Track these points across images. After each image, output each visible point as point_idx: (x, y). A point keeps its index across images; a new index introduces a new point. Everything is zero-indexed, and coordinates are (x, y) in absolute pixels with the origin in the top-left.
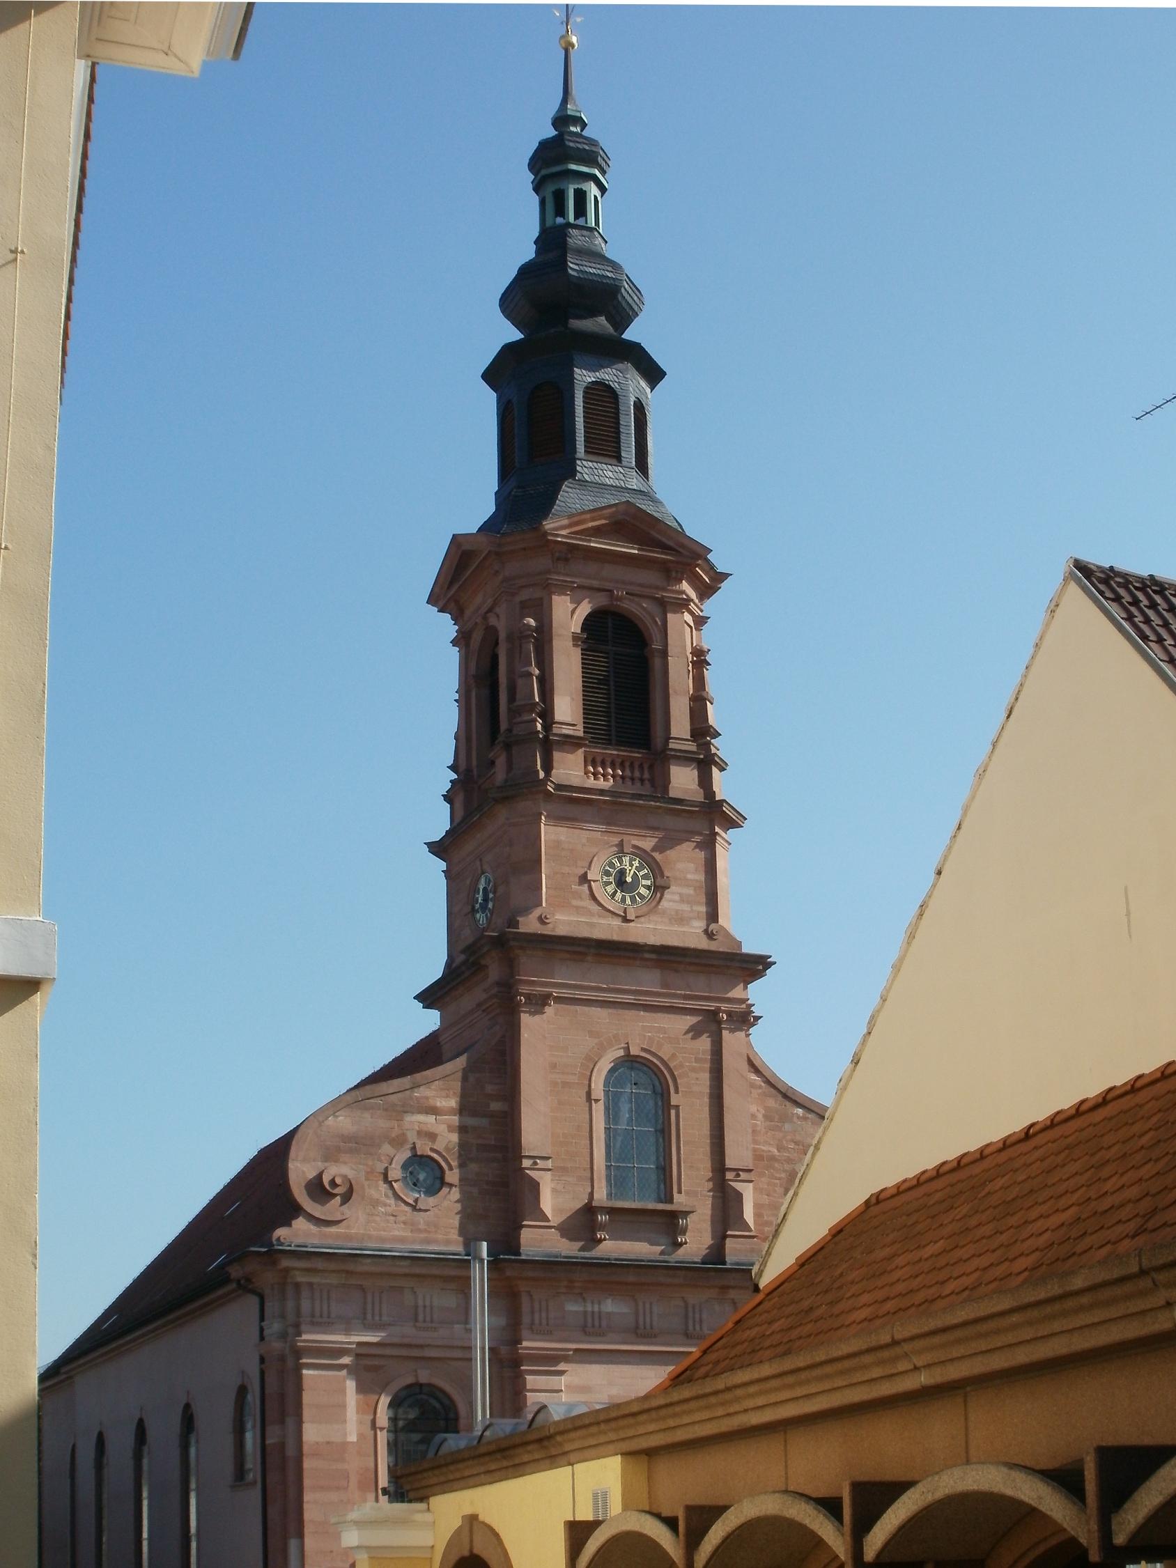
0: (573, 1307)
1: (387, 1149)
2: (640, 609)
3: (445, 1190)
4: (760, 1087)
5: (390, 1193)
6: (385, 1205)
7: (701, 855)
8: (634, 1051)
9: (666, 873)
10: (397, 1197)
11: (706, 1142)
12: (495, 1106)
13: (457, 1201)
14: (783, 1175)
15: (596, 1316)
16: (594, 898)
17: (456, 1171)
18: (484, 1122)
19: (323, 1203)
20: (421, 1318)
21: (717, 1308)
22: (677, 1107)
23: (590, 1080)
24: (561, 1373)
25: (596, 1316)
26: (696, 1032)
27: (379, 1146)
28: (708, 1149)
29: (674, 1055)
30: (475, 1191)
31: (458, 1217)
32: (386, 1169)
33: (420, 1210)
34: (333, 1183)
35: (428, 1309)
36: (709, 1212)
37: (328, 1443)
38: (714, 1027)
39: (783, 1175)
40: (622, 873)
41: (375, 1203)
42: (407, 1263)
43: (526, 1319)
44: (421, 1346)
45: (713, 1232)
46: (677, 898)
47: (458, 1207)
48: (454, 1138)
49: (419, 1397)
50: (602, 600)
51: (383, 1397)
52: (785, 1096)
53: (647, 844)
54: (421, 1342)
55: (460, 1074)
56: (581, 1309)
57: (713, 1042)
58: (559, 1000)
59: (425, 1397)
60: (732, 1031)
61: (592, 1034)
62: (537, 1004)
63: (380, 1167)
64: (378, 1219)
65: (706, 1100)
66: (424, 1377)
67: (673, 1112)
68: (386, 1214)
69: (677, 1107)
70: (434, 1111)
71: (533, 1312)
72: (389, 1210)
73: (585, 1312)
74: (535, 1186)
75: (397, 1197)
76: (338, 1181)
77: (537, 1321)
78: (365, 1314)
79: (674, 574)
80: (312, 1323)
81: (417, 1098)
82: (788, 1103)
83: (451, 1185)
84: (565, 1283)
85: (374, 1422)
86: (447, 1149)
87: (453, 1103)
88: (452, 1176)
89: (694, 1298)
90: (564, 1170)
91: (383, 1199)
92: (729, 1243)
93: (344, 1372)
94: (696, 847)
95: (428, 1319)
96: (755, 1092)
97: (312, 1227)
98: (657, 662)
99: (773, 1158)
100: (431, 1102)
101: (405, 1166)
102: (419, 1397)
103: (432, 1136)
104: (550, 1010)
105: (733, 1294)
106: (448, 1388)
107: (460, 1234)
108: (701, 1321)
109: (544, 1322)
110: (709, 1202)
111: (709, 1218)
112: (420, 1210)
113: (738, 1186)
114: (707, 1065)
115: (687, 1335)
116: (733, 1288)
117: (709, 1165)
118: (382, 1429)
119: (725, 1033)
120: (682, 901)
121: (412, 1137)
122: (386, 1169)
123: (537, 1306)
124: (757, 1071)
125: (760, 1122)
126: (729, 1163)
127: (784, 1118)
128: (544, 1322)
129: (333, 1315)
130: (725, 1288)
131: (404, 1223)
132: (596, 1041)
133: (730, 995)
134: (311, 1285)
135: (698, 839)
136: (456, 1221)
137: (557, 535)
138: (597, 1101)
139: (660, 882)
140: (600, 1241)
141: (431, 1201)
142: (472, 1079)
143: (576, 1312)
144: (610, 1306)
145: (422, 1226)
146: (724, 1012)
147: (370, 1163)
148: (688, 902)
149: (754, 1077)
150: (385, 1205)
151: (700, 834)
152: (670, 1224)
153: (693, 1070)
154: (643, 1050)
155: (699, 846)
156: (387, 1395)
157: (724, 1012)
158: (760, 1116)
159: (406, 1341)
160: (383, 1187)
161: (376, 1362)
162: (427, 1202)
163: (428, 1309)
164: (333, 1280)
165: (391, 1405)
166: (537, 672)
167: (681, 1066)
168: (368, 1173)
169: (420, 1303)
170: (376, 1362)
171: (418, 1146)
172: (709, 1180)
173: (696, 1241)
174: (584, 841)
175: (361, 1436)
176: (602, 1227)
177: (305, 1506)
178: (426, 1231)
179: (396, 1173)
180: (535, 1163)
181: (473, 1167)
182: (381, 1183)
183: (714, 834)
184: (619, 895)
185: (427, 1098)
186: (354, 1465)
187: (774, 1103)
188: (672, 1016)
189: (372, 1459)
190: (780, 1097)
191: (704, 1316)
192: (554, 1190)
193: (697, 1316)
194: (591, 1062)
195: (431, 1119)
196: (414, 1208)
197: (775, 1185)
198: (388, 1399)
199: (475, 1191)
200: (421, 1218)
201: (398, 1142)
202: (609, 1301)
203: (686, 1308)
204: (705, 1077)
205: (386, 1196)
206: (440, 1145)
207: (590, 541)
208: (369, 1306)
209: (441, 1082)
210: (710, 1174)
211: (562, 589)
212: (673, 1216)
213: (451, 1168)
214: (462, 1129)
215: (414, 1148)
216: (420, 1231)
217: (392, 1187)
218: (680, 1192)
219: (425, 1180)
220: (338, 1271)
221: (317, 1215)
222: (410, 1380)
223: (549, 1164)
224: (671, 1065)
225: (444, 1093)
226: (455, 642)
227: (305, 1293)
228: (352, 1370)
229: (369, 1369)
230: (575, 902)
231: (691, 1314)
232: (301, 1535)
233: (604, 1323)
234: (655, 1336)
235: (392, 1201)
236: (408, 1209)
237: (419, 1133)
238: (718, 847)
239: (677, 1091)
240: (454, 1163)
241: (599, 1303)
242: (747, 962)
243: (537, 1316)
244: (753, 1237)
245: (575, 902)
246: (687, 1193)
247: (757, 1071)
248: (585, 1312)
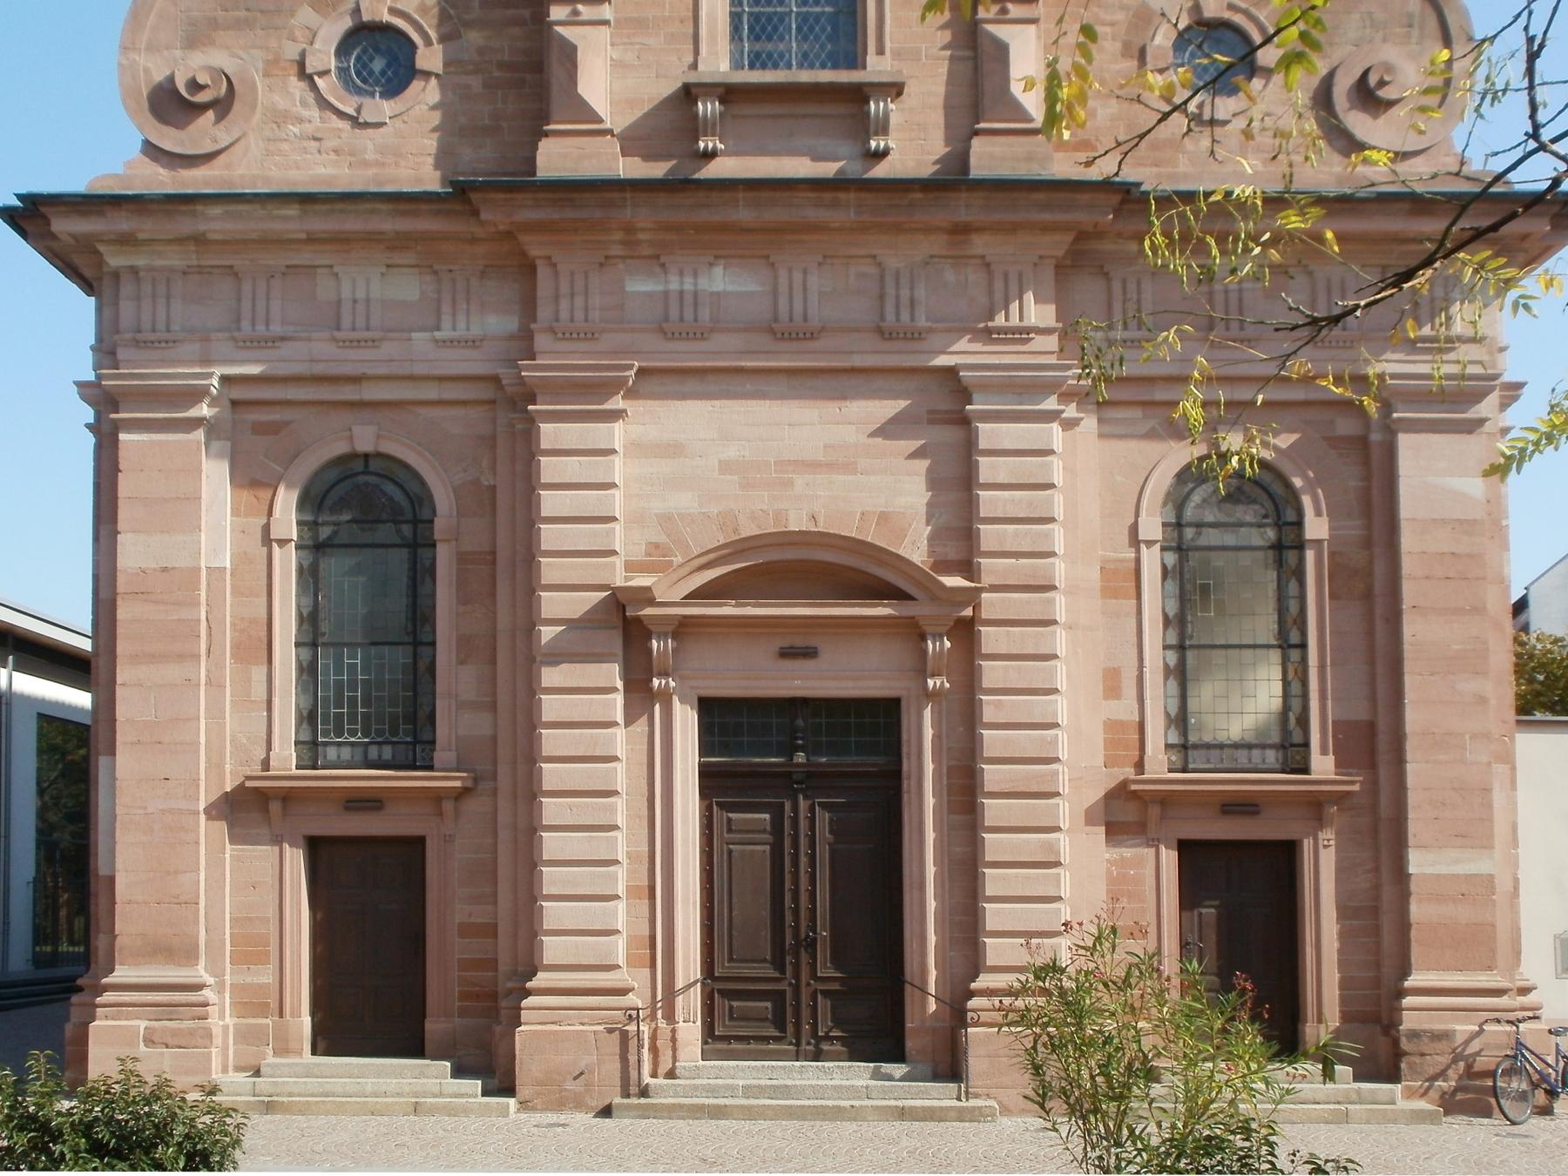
0: (640, 285)
3: (417, 85)
5: (310, 98)
6: (301, 120)
10: (324, 104)
13: (434, 108)
15: (689, 300)
17: (438, 48)
19: (181, 125)
20: (346, 321)
21: (950, 276)
24: (616, 415)
25: (689, 300)
30: (475, 83)
31: (436, 135)
32: (303, 54)
33: (367, 125)
34: (195, 86)
35: (361, 308)
36: (941, 90)
37: (165, 570)
39: (1120, 16)
41: (280, 118)
42: (292, 211)
43: (544, 312)
44: (356, 380)
45: (948, 126)
47: (436, 118)
49: (362, 479)
51: (281, 490)
54: (348, 369)
56: (660, 288)
59: (372, 479)
63: (291, 51)
64: (285, 146)
66: (365, 439)
68: (302, 137)
71: (557, 298)
73: (666, 293)
75: (324, 104)
76: (203, 79)
77: (564, 315)
78: (238, 320)
80: (137, 343)
83: (427, 75)
84: (618, 236)
85: (266, 529)
88: (430, 57)
89: (898, 256)
90: (640, 24)
93: (200, 435)
95: (361, 322)
97: (161, 170)
101: (343, 49)
102: (362, 479)
105: (980, 244)
106: (412, 459)
107: (437, 166)
108: (912, 303)
109: (579, 315)
110: (943, 69)
111: (940, 101)
112: (367, 125)
113: (1001, 31)
115: (883, 333)
118: (283, 542)
122: (303, 54)
123: (564, 288)
128: (579, 315)
129: (175, 327)
130: (961, 231)
131: (335, 151)
134: (134, 270)
136: (431, 143)
140: (710, 155)
141: (387, 107)
143: (649, 295)
144: (719, 280)
145: (370, 156)
147: (273, 44)
150: (301, 120)
152: (852, 107)
156: (289, 486)
159: (319, 369)
160: (297, 87)
161: (274, 416)
162: (380, 108)
163: (361, 308)
164: (173, 259)
165: (302, 504)
168: (267, 63)
169: (346, 293)
170: (274, 416)
173: (911, 142)
175: (240, 559)
176: (707, 128)
177: (119, 691)
178: (378, 164)
179: (324, 56)
181: (474, 37)
182: (294, 80)
186: (220, 614)
189: (264, 599)
191: (921, 293)
192: (617, 65)
193: (905, 293)
196: (355, 121)
198: (294, 496)
199: (475, 83)
200: (368, 141)
202: (718, 271)
203: (882, 278)
205: (304, 103)
208: (246, 305)
212: (858, 95)
213: (428, 43)
216: (366, 164)
217: (314, 87)
218: (881, 51)
219: (383, 73)
220: (180, 241)
221: (167, 146)
222: (341, 448)
227: (127, 289)
228: (212, 428)
229: (260, 429)
231: (890, 290)
232: (112, 751)
233: (705, 314)
234: (812, 336)
235: (314, 113)
236: (345, 125)
240: (433, 34)
241: (695, 275)
243: (564, 304)
244: (1035, 132)
246: (897, 54)
248: (666, 293)
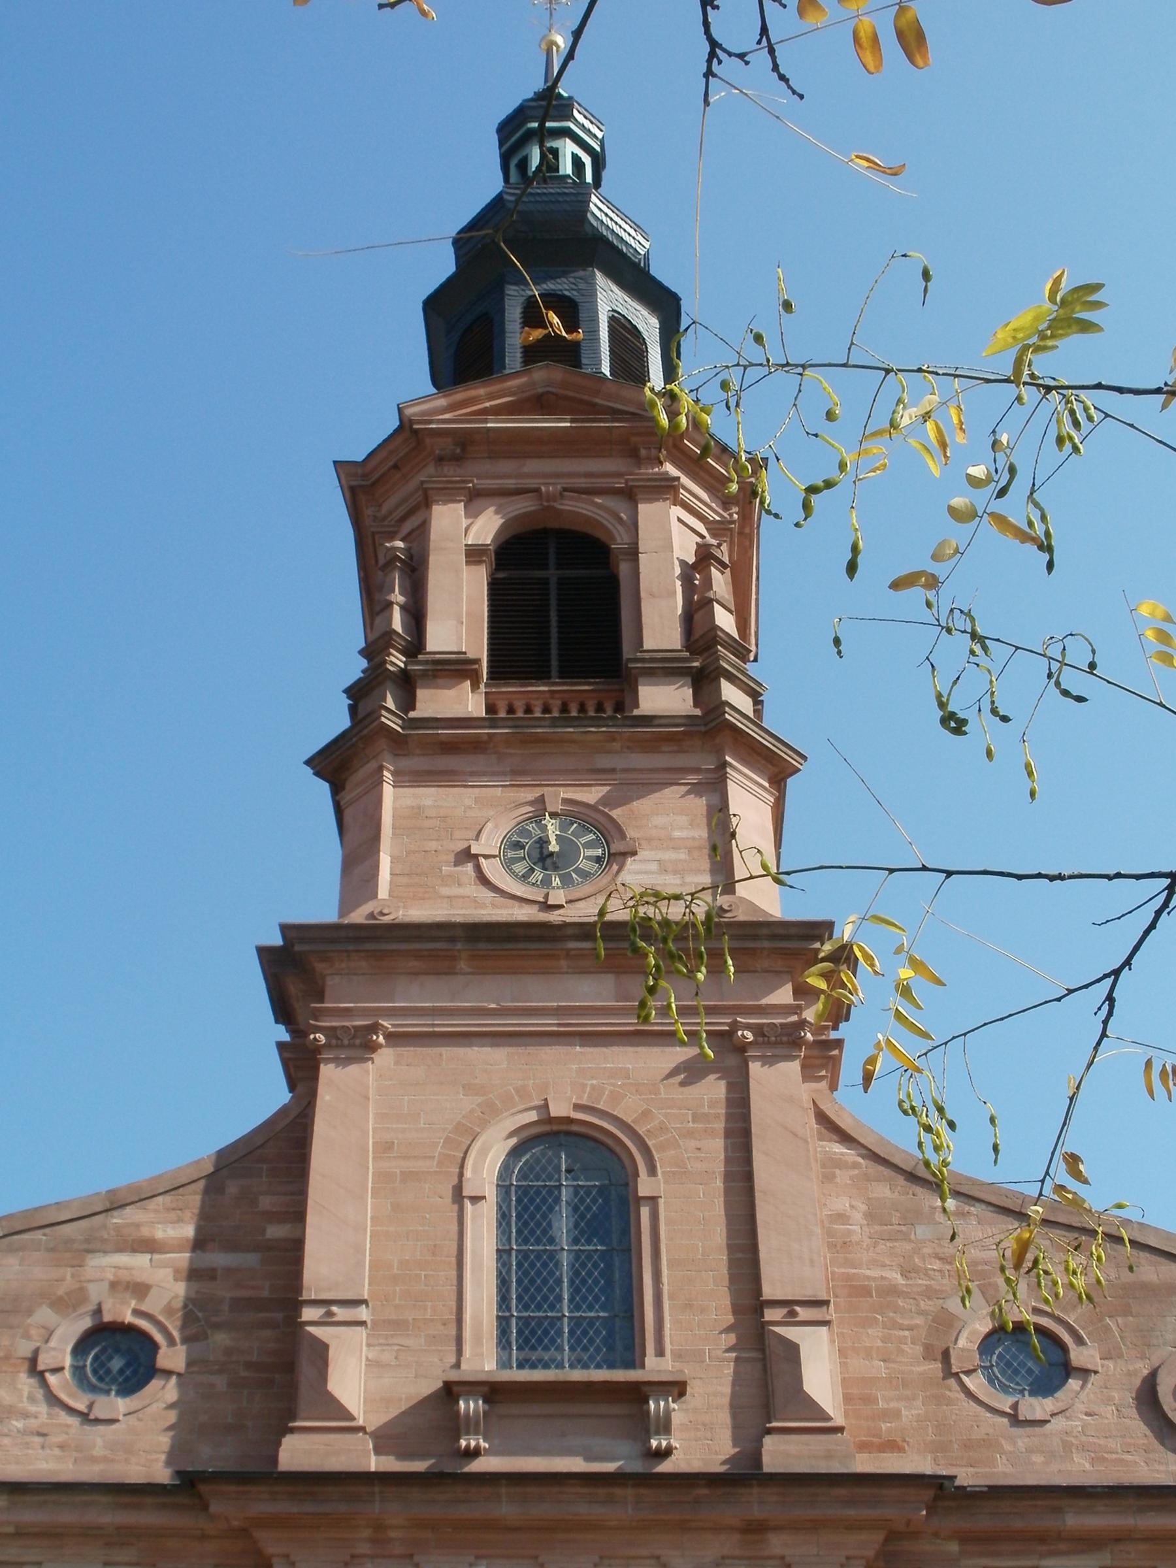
1: (44, 1315)
2: (593, 510)
4: (856, 1165)
5: (39, 1394)
6: (26, 1415)
7: (699, 804)
8: (556, 1110)
9: (631, 833)
11: (721, 1261)
12: (275, 1231)
14: (919, 1321)
16: (484, 880)
18: (250, 1260)
22: (653, 1200)
23: (462, 1166)
26: (691, 1072)
27: (30, 1312)
28: (725, 1271)
29: (646, 1114)
32: (36, 1352)
33: (97, 1421)
36: (727, 1390)
38: (732, 1061)
39: (919, 1321)
40: (543, 842)
46: (654, 867)
48: (180, 1289)
50: (523, 505)
52: (912, 1177)
53: (591, 795)
55: (201, 1184)
57: (730, 1087)
58: (394, 1038)
60: (768, 1061)
61: (469, 1089)
62: (351, 1046)
63: (24, 1348)
65: (719, 1183)
67: (645, 1212)
68: (25, 1432)
69: (653, 1200)
70: (149, 1246)
72: (33, 1423)
74: (321, 1351)
79: (643, 452)
81: (118, 1228)
82: (919, 1190)
83: (168, 1373)
84: (366, 1533)
86: (169, 1311)
87: (188, 1231)
88: (172, 1357)
90: (398, 1325)
91: (26, 1405)
92: (769, 1442)
94: (688, 792)
96: (843, 1177)
98: (624, 568)
99: (893, 1290)
100: (145, 1232)
101: (81, 1347)
103: (141, 1290)
104: (385, 1057)
111: (726, 1401)
112: (97, 1421)
113: (790, 1333)
114: (720, 1125)
116: (777, 1529)
117: (726, 1302)
119: (755, 1067)
120: (664, 870)
121: (97, 1292)
122: (36, 1352)
124: (845, 1138)
125: (857, 1228)
126: (769, 1291)
127: (912, 1217)
130: (755, 1529)
131: (61, 1447)
132: (480, 1099)
133: (765, 1001)
135: (693, 779)
136: (165, 1440)
137: (430, 422)
138: (475, 1199)
139: (617, 847)
141: (122, 1405)
142: (232, 1188)
145: (98, 1451)
146: (748, 1027)
148: (675, 872)
149: (838, 1149)
150: (26, 1415)
151: (696, 770)
153: (690, 1134)
154: (577, 1107)
155: (696, 789)
157: (748, 1027)
158: (858, 1216)
160: (26, 1383)
166: (401, 599)
167: (662, 1129)
171: (106, 1308)
172: (728, 1330)
173: (697, 1437)
174: (469, 802)
178: (105, 1459)
180: (330, 1314)
183: (724, 765)
184: (538, 875)
185: (138, 1226)
187: (887, 1190)
188: (642, 1050)
190: (901, 1180)
194: (465, 1137)
195: (142, 1260)
197: (902, 1341)
199: (220, 1382)
201: (65, 1304)
204: (716, 1146)
205: (32, 1399)
206: (153, 1304)
207: (486, 421)
209: (167, 1199)
210: (730, 1319)
211: (449, 493)
212: (638, 1393)
213: (171, 1342)
214: (194, 1274)
215: (98, 1311)
216: (94, 1460)
217: (44, 1384)
218: (660, 1353)
223: (363, 1313)
224: (641, 1131)
225: (173, 1215)
226: (363, 652)
230: (445, 891)
235: (42, 1409)
236: (74, 1421)
237: (114, 1285)
238: (731, 787)
239: (652, 1171)
242: (788, 937)
245: (445, 891)
247: (845, 1138)
